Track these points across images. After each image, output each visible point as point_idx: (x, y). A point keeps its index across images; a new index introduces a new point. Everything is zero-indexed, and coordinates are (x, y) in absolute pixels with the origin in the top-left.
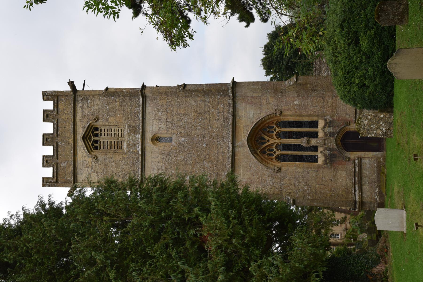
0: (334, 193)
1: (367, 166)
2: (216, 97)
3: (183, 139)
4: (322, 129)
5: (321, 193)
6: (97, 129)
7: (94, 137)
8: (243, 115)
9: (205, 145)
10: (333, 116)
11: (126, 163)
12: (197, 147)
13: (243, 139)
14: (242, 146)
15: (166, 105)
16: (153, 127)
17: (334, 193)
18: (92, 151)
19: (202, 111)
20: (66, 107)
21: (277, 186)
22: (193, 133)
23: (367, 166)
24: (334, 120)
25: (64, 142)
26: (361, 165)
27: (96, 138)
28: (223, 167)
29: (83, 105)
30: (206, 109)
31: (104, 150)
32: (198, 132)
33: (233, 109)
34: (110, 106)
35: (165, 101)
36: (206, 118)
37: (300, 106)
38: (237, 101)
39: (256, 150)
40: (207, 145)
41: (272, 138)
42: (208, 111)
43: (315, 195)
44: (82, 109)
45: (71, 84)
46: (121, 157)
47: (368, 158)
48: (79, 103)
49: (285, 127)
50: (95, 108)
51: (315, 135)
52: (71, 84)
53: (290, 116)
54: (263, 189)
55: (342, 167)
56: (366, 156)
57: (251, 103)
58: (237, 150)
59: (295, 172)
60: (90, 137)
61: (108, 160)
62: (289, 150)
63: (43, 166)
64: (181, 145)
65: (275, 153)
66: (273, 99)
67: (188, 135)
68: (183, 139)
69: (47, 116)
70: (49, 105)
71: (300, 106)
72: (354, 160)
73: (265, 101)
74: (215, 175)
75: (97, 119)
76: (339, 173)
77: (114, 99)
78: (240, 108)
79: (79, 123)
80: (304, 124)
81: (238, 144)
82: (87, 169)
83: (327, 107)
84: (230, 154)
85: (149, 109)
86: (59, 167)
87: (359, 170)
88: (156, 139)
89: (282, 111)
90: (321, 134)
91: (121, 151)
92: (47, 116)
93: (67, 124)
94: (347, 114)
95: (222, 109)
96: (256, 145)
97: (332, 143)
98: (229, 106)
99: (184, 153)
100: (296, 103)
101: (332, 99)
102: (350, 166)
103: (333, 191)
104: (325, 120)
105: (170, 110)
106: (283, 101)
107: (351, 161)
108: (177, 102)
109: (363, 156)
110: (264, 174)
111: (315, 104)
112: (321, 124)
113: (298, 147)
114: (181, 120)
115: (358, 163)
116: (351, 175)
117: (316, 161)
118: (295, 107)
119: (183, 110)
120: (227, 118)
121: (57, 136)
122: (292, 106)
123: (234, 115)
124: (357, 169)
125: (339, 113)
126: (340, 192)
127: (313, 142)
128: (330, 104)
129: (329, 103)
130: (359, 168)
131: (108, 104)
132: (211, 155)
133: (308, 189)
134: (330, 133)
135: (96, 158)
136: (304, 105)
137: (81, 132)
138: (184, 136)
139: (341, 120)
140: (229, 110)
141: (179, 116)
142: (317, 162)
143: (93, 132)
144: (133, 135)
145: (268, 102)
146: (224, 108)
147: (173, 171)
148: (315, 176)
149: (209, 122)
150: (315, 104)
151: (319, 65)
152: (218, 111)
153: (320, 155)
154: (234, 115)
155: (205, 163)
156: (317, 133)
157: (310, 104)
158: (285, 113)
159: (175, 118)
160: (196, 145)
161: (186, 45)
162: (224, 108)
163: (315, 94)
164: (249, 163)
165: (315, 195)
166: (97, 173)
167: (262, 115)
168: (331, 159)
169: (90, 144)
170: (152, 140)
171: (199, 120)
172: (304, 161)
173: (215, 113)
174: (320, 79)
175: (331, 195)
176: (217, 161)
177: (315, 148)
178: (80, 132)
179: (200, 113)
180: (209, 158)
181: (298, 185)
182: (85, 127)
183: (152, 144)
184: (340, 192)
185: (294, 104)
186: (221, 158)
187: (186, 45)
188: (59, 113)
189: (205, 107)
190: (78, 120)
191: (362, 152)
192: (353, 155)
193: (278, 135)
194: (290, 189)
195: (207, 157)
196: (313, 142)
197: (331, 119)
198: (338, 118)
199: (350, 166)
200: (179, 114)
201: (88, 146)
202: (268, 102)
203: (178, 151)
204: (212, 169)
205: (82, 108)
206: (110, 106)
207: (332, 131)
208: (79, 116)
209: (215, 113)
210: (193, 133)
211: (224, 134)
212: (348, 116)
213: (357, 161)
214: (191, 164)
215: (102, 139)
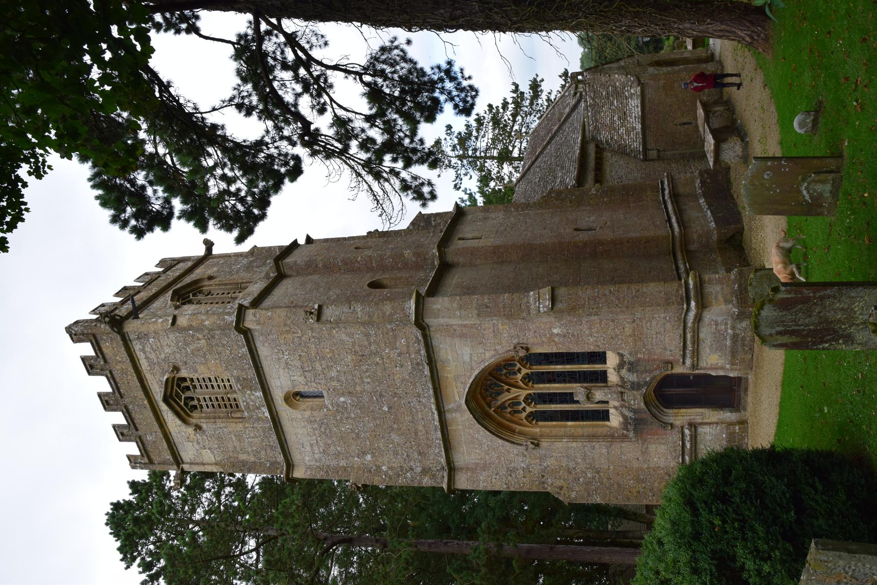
0: (644, 485)
1: (708, 437)
2: (389, 327)
3: (342, 399)
4: (614, 369)
5: (619, 486)
7: (183, 393)
8: (450, 358)
9: (385, 409)
10: (636, 354)
11: (252, 435)
12: (373, 411)
13: (457, 398)
14: (458, 409)
15: (293, 343)
16: (281, 382)
17: (644, 485)
18: (189, 416)
19: (367, 352)
20: (113, 347)
21: (536, 470)
22: (358, 388)
23: (708, 437)
24: (639, 360)
25: (138, 406)
26: (696, 437)
27: (188, 394)
28: (429, 442)
29: (144, 347)
30: (373, 348)
31: (209, 410)
32: (368, 387)
33: (428, 351)
34: (191, 347)
35: (289, 336)
36: (378, 363)
37: (564, 336)
38: (432, 334)
39: (487, 408)
40: (390, 408)
42: (377, 352)
43: (608, 492)
44: (145, 353)
46: (241, 425)
47: (710, 424)
48: (134, 343)
49: (540, 364)
50: (167, 351)
54: (510, 478)
55: (658, 439)
56: (706, 421)
57: (462, 336)
58: (449, 416)
59: (568, 448)
60: (177, 395)
61: (220, 431)
64: (341, 409)
65: (524, 409)
66: (507, 327)
67: (350, 393)
68: (342, 399)
71: (564, 336)
72: (682, 428)
73: (491, 330)
74: (416, 454)
75: (176, 369)
76: (652, 448)
77: (193, 336)
78: (441, 346)
79: (148, 377)
80: (578, 357)
81: (449, 406)
82: (190, 444)
83: (623, 338)
84: (437, 423)
85: (264, 351)
86: (146, 443)
87: (691, 447)
88: (294, 397)
89: (529, 346)
90: (613, 377)
91: (239, 415)
93: (130, 377)
94: (665, 349)
95: (405, 349)
96: (484, 399)
97: (636, 400)
98: (418, 341)
99: (350, 421)
100: (555, 331)
101: (634, 321)
102: (674, 437)
103: (643, 481)
104: (621, 356)
105: (302, 351)
106: (529, 330)
107: (676, 429)
108: (314, 337)
109: (699, 420)
110: (509, 452)
111: (598, 332)
112: (612, 360)
113: (568, 398)
114: (329, 368)
115: (691, 436)
116: (675, 450)
117: (607, 418)
118: (556, 339)
119: (328, 350)
120: (418, 364)
121: (122, 397)
122: (550, 338)
123: (431, 360)
124: (688, 445)
125: (650, 347)
126: (656, 484)
128: (628, 330)
129: (626, 329)
130: (691, 444)
131: (187, 344)
132: (403, 423)
133: (594, 478)
134: (633, 383)
135: (198, 428)
136: (573, 335)
137: (158, 390)
138: (343, 395)
139: (655, 360)
140: (420, 350)
141: (323, 362)
142: (608, 420)
143: (179, 386)
144: (248, 392)
145: (496, 333)
146: (408, 347)
147: (339, 449)
148: (606, 454)
149: (385, 370)
150: (598, 332)
151: (593, 99)
152: (398, 351)
153: (612, 411)
154: (431, 360)
155: (393, 436)
157: (587, 332)
159: (317, 365)
160: (368, 408)
162: (408, 347)
164: (476, 436)
165: (608, 492)
166: (210, 449)
168: (636, 425)
169: (182, 404)
170: (287, 399)
171: (364, 368)
172: (583, 419)
173: (393, 354)
174: (604, 295)
175: (639, 492)
176: (416, 434)
178: (158, 393)
179: (363, 355)
180: (399, 429)
181: (574, 468)
182: (161, 381)
183: (287, 407)
184: (656, 484)
185: (552, 334)
186: (420, 428)
188: (108, 360)
189: (370, 344)
190: (145, 372)
191: (698, 410)
194: (560, 478)
195: (396, 426)
197: (632, 359)
198: (646, 357)
199: (674, 437)
200: (323, 358)
201: (179, 409)
202: (496, 333)
203: (338, 418)
204: (408, 444)
205: (143, 350)
206: (191, 347)
207: (636, 380)
208: (144, 365)
209: (393, 354)
210: (358, 388)
211: (419, 390)
212: (669, 353)
213: (687, 432)
214: (368, 438)
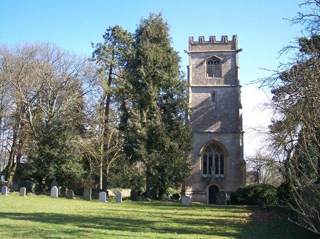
6: (218, 63)
41: (215, 152)
45: (240, 50)
51: (217, 173)
52: (240, 50)
53: (227, 161)
62: (209, 160)
63: (227, 36)
69: (224, 38)
70: (230, 39)
90: (217, 176)
92: (224, 38)
112: (222, 176)
127: (213, 172)
156: (218, 174)
158: (228, 158)
161: (171, 38)
163: (237, 173)
167: (227, 147)
177: (210, 173)
187: (171, 38)
192: (207, 190)
193: (216, 155)
196: (213, 172)
215: (213, 65)
